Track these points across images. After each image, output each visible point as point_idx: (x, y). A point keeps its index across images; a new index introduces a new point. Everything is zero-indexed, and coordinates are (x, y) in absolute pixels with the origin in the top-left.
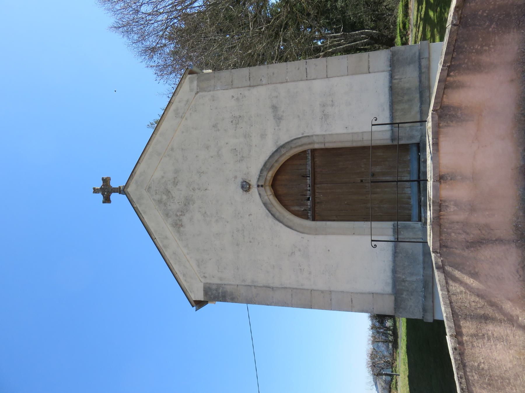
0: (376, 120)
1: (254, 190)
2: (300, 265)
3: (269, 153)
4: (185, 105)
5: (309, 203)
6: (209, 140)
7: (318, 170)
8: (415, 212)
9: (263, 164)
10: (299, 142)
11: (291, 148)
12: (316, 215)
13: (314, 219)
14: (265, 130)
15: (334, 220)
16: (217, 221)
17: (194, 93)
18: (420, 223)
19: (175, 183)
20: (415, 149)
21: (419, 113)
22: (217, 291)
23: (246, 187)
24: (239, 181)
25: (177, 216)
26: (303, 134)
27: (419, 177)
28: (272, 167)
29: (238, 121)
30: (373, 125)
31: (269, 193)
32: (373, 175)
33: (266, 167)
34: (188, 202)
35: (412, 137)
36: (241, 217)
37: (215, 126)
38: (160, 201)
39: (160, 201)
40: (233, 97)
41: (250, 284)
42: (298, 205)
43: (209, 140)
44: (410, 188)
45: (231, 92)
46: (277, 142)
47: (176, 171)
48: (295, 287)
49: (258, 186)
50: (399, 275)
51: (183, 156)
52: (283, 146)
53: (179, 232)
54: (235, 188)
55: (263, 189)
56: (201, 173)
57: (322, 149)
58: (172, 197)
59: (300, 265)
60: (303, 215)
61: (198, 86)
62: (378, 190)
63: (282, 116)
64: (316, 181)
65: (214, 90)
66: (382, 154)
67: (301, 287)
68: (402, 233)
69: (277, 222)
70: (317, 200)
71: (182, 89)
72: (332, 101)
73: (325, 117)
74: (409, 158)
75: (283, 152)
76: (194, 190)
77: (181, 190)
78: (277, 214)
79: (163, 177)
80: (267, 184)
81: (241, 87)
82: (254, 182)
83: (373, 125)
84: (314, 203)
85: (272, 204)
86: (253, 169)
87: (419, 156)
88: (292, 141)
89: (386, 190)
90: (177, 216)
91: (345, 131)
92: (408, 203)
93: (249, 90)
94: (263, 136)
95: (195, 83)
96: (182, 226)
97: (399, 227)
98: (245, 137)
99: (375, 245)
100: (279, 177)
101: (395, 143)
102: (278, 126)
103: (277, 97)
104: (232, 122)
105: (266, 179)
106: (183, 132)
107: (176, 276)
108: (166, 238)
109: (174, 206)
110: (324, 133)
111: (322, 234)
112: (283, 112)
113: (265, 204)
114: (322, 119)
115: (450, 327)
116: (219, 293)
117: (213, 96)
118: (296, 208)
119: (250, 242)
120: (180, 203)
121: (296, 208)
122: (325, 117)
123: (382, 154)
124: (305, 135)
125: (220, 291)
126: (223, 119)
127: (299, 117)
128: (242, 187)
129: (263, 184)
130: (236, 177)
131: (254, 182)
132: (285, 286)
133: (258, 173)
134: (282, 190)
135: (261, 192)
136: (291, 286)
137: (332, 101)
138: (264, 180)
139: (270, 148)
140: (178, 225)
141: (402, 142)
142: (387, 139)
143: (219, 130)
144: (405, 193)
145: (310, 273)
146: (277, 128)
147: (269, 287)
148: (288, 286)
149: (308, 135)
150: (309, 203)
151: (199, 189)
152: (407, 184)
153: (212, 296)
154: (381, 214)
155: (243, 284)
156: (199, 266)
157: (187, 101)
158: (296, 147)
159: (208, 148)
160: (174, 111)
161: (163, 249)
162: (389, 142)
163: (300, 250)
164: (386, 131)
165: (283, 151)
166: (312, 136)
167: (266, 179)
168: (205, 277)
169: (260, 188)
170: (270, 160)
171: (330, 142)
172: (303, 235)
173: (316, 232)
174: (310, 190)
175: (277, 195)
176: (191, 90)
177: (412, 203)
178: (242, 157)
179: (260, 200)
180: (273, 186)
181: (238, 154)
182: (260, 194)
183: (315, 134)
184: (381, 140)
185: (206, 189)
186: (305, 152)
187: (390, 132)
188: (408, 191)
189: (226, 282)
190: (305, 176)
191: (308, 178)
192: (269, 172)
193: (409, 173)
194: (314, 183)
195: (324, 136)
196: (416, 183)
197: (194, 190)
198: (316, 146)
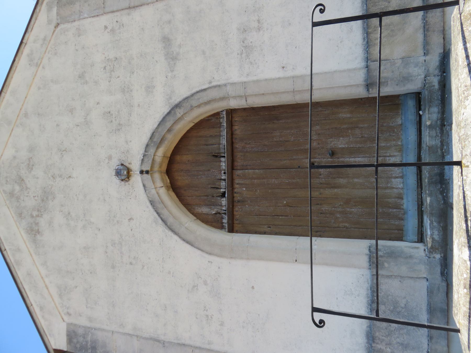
0: (322, 11)
1: (137, 179)
2: (205, 309)
3: (158, 117)
4: (42, 45)
5: (224, 201)
6: (73, 100)
7: (238, 145)
8: (411, 224)
9: (149, 135)
10: (205, 97)
11: (192, 108)
12: (235, 222)
13: (231, 230)
14: (153, 78)
15: (265, 233)
16: (84, 227)
17: (52, 27)
18: (420, 245)
19: (30, 167)
20: (411, 104)
21: (421, 31)
22: (84, 338)
23: (124, 173)
24: (115, 164)
25: (32, 216)
26: (210, 82)
27: (419, 158)
28: (162, 140)
29: (114, 65)
30: (315, 24)
31: (159, 183)
32: (333, 154)
33: (155, 140)
34: (47, 195)
35: (406, 79)
36: (118, 222)
37: (81, 76)
38: (11, 194)
39: (11, 194)
40: (106, 27)
41: (131, 332)
42: (207, 205)
43: (73, 100)
44: (402, 177)
45: (104, 20)
46: (171, 98)
47: (31, 149)
48: (198, 344)
49: (142, 172)
50: (379, 346)
51: (40, 125)
52: (178, 106)
53: (34, 241)
54: (107, 174)
55: (148, 176)
56: (63, 151)
57: (244, 109)
58: (27, 188)
59: (205, 309)
60: (213, 222)
61: (58, 14)
62: (342, 181)
63: (178, 54)
64: (236, 164)
65: (79, 19)
66: (348, 115)
67: (208, 347)
68: (386, 265)
69: (170, 233)
70: (237, 197)
71: (37, 22)
72: (259, 21)
73: (247, 49)
74: (400, 122)
75: (179, 115)
76: (54, 178)
77: (38, 178)
78: (170, 220)
79: (15, 157)
80: (156, 168)
81: (117, 11)
82: (136, 166)
83: (315, 24)
84: (232, 203)
85: (162, 202)
86: (134, 144)
87: (420, 116)
88: (192, 95)
89: (356, 180)
90: (32, 216)
91: (281, 74)
92: (398, 207)
93: (129, 14)
94: (149, 89)
95: (55, 10)
96: (38, 232)
97: (380, 253)
98: (123, 91)
99: (322, 321)
100: (178, 158)
101: (374, 93)
102: (172, 71)
103: (170, 22)
104: (105, 68)
105: (153, 160)
106: (39, 88)
107: (31, 308)
108: (19, 250)
109: (29, 202)
110: (244, 79)
111: (242, 258)
112: (180, 46)
113: (152, 203)
114: (241, 54)
115: (458, 210)
116: (87, 342)
117: (78, 29)
118: (205, 210)
119: (131, 264)
120: (36, 198)
121: (205, 210)
122: (247, 49)
123: (348, 115)
124: (214, 84)
125: (89, 339)
126: (92, 65)
127: (204, 53)
128: (118, 173)
129: (149, 169)
130: (110, 158)
131: (136, 166)
132: (183, 342)
133: (142, 151)
134: (182, 180)
135: (146, 183)
136: (191, 343)
137: (259, 21)
138: (150, 162)
139: (159, 109)
140: (34, 231)
141: (387, 90)
142: (357, 86)
143: (86, 83)
144: (393, 188)
145: (222, 324)
146: (170, 74)
147: (159, 341)
148: (188, 342)
149: (219, 83)
150: (224, 201)
151: (61, 176)
152: (397, 170)
153: (78, 346)
154: (347, 225)
155: (121, 330)
156: (60, 296)
157: (44, 39)
158: (199, 106)
159: (72, 111)
160: (28, 55)
161: (15, 266)
162: (361, 92)
163: (205, 283)
164: (355, 69)
165: (179, 113)
166: (225, 85)
167: (153, 160)
168: (69, 314)
169: (145, 175)
170: (160, 130)
171: (256, 95)
172: (212, 258)
173: (231, 253)
174: (225, 180)
175: (175, 188)
176: (49, 22)
177: (405, 206)
178: (120, 124)
179: (145, 195)
180: (169, 172)
181: (114, 120)
182: (144, 186)
183: (230, 81)
184: (345, 87)
185: (70, 177)
186: (217, 115)
187: (365, 71)
188: (397, 183)
189: (98, 326)
190: (217, 156)
191: (223, 159)
192: (158, 148)
193: (401, 150)
194: (232, 167)
195: (244, 84)
196: (413, 169)
197: (54, 177)
198: (234, 104)
